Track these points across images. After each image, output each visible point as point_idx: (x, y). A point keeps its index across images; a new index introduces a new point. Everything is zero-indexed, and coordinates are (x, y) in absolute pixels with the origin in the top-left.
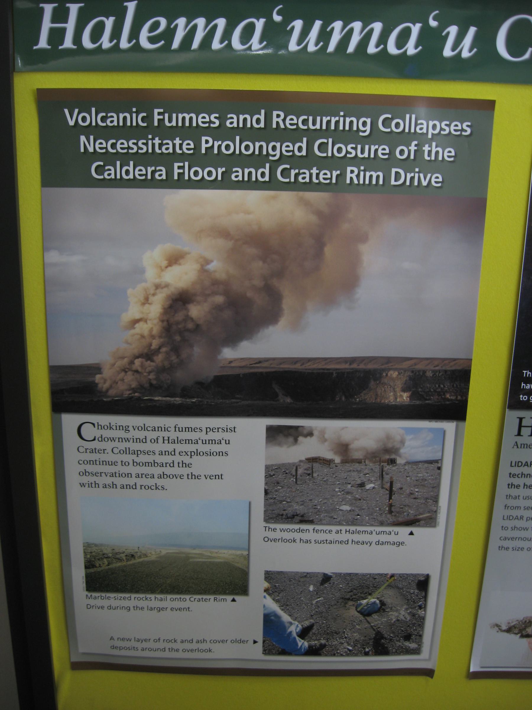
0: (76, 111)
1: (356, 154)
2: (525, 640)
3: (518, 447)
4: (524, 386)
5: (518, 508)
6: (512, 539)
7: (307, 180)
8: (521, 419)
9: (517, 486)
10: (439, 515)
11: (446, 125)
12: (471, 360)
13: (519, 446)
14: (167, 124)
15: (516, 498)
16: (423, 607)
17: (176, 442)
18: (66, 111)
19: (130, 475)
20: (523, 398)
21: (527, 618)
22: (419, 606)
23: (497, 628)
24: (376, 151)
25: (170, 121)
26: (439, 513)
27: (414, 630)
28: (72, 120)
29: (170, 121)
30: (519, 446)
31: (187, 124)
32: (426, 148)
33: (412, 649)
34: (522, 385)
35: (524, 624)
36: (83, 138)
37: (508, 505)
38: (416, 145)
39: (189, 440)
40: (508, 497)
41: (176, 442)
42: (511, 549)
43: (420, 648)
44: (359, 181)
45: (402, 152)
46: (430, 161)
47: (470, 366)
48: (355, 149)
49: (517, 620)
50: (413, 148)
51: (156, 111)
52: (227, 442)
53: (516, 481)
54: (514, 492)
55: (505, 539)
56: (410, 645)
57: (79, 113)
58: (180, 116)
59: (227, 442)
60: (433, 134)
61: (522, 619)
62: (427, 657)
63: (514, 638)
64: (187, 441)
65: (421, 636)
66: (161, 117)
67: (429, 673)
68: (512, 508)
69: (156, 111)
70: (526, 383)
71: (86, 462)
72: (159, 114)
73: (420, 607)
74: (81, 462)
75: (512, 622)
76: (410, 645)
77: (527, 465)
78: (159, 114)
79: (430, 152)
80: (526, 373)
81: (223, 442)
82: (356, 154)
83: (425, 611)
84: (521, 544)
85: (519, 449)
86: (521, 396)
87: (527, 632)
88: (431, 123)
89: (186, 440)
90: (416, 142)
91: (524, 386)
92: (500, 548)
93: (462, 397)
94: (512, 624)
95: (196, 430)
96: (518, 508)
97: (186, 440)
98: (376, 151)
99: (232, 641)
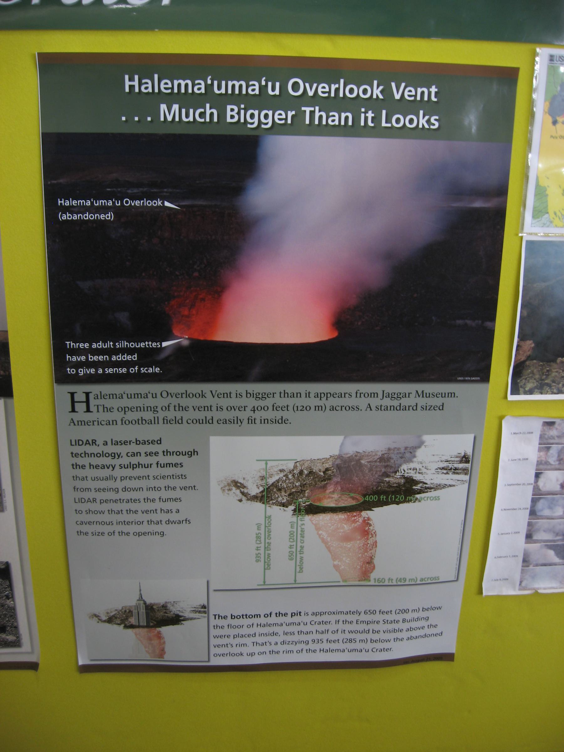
0: (403, 85)
2: (130, 631)
3: (75, 425)
4: (69, 358)
5: (89, 489)
6: (89, 523)
8: (72, 394)
9: (82, 467)
10: (4, 499)
12: (7, 331)
13: (76, 423)
14: (216, 91)
15: (83, 479)
16: (11, 596)
17: (99, 397)
18: (393, 84)
20: (71, 371)
21: (125, 607)
22: (5, 595)
23: (97, 619)
25: (219, 88)
26: (5, 497)
27: (7, 621)
28: (398, 93)
29: (219, 88)
30: (76, 423)
31: (183, 91)
33: (11, 642)
34: (68, 357)
35: (124, 614)
36: (163, 107)
37: (76, 487)
39: (138, 394)
40: (75, 478)
41: (99, 397)
42: (90, 534)
43: (19, 640)
47: (7, 339)
49: (116, 610)
50: (136, 368)
52: (154, 396)
53: (80, 461)
54: (80, 473)
55: (82, 523)
56: (8, 637)
58: (230, 84)
59: (154, 396)
61: (120, 608)
62: (29, 650)
63: (117, 630)
64: (111, 396)
65: (16, 628)
67: (33, 666)
68: (82, 490)
70: (71, 355)
73: (8, 597)
75: (111, 612)
76: (8, 637)
77: (89, 444)
80: (70, 344)
81: (150, 396)
83: (14, 600)
84: (100, 528)
85: (77, 427)
86: (68, 369)
87: (130, 622)
91: (69, 358)
92: (79, 533)
93: (4, 372)
94: (112, 614)
96: (89, 489)
99: (141, 594)
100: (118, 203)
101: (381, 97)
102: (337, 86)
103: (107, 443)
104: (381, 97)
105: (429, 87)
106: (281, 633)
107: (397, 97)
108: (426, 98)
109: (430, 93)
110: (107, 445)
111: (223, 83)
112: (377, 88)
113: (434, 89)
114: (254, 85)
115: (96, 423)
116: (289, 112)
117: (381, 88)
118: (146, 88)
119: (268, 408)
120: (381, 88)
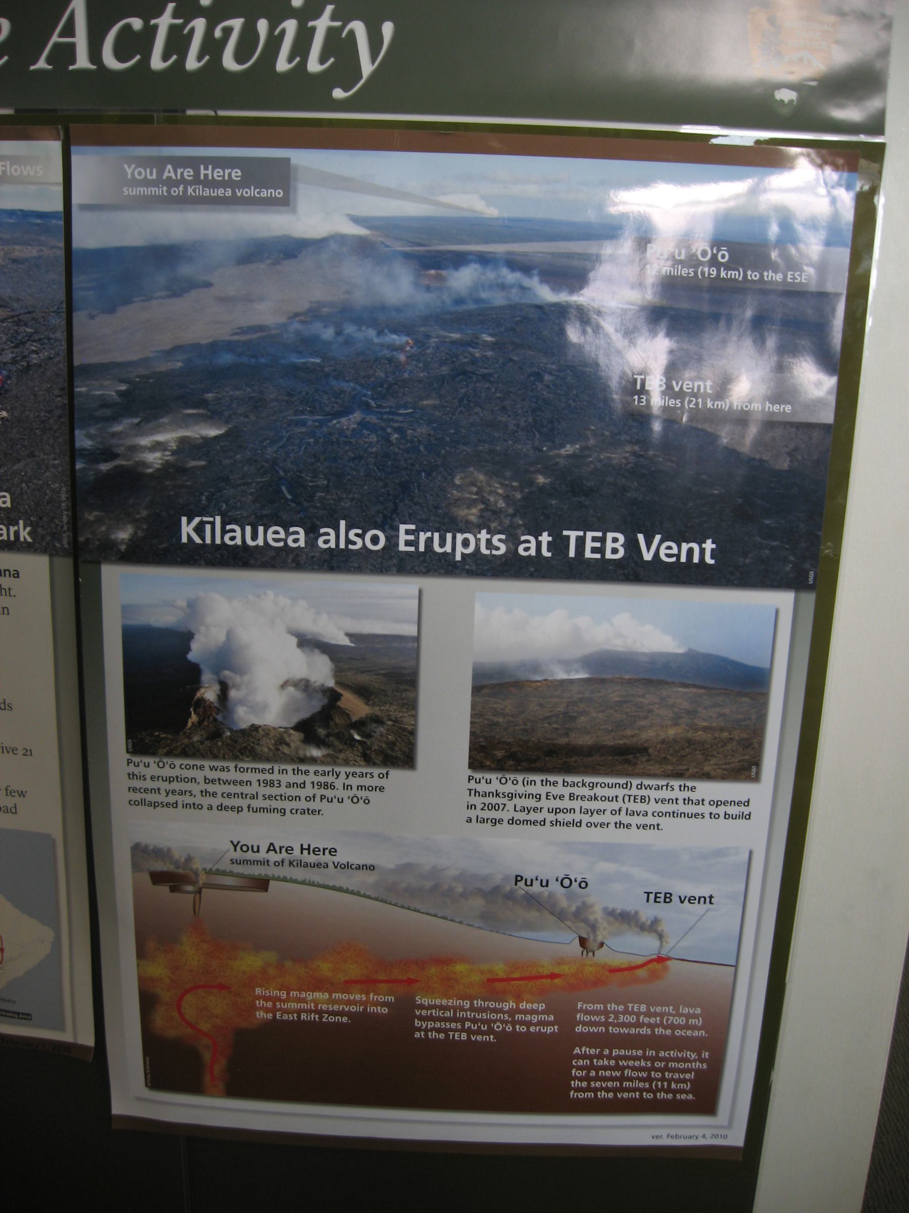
0: (658, 538)
1: (364, 543)
7: (533, 552)
11: (357, 535)
18: (641, 537)
28: (648, 549)
44: (203, 539)
48: (349, 542)
51: (403, 528)
57: (662, 541)
66: (412, 537)
69: (403, 528)
72: (408, 532)
78: (408, 532)
82: (364, 543)
101: (29, 540)
102: (16, 528)
104: (29, 540)
105: (701, 542)
106: (201, 779)
107: (648, 556)
108: (696, 560)
109: (702, 551)
111: (449, 536)
113: (709, 545)
114: (528, 541)
117: (28, 529)
120: (28, 529)
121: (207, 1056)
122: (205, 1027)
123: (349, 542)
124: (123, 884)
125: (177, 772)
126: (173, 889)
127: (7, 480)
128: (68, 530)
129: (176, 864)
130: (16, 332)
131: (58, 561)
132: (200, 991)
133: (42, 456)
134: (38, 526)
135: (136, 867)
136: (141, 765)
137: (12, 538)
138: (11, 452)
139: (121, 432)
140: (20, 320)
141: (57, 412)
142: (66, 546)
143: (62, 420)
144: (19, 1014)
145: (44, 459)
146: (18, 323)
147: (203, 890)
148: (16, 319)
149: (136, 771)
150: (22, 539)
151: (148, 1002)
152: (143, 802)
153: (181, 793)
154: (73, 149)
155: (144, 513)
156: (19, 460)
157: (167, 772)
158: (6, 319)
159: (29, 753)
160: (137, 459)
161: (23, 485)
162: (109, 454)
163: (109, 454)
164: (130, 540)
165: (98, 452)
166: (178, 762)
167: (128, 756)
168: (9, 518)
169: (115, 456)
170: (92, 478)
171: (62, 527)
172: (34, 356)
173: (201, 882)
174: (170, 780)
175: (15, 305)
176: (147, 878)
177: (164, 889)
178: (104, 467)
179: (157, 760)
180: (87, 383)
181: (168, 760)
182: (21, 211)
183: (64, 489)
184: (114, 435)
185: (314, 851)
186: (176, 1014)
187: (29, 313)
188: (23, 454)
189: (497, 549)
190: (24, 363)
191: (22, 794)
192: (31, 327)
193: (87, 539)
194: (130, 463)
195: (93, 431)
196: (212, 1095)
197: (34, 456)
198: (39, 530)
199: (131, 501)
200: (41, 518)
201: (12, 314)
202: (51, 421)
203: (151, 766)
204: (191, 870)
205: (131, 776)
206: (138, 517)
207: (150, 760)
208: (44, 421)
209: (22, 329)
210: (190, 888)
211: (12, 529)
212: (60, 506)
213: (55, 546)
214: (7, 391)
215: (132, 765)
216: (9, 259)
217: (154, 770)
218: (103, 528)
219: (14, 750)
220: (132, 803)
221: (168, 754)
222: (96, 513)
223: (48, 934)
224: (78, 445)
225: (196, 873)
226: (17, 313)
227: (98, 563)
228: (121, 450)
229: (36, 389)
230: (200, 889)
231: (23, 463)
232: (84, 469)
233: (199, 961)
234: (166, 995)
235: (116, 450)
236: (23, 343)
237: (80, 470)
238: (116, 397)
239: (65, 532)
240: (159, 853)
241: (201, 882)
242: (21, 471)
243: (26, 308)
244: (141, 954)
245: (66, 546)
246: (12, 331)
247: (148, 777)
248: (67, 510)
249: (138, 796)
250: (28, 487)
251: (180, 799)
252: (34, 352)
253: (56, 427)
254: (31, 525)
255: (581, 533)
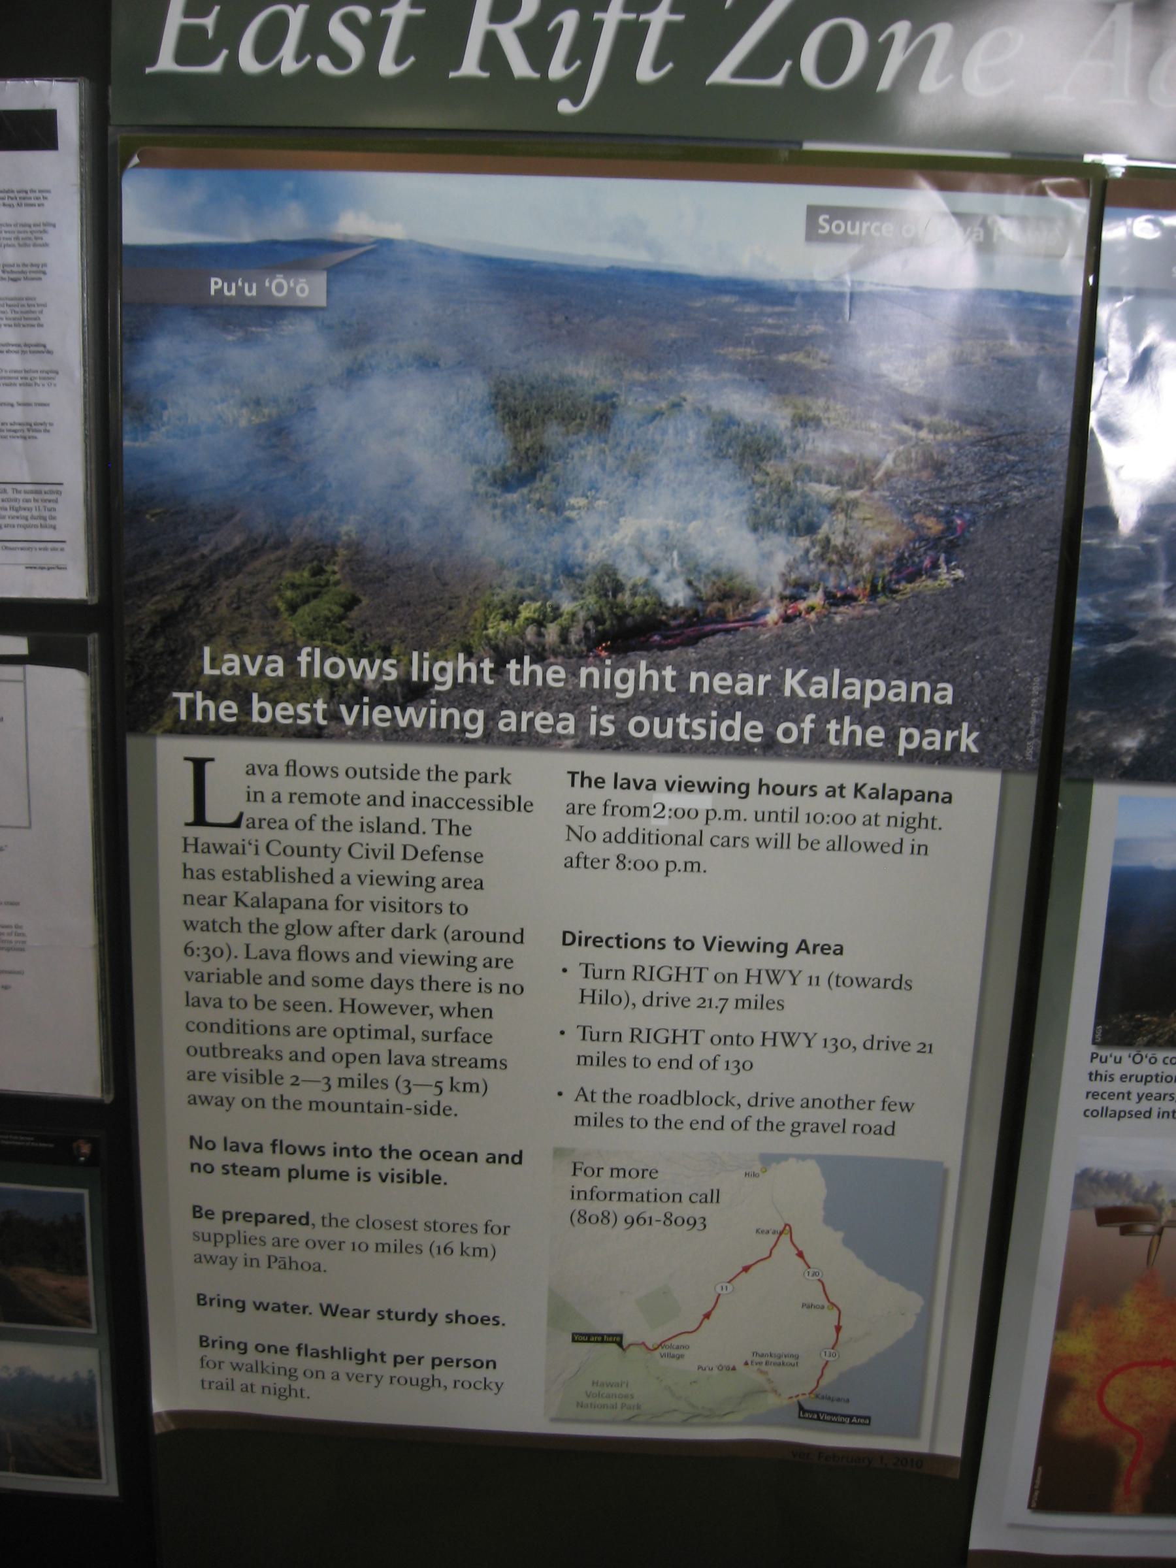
19: (260, 1103)
24: (531, 722)
32: (833, 726)
38: (812, 721)
45: (787, 733)
46: (839, 747)
50: (807, 725)
60: (873, 703)
64: (315, 798)
71: (202, 1027)
74: (192, 1027)
79: (839, 734)
88: (869, 684)
89: (312, 795)
90: (813, 716)
95: (375, 1085)
97: (312, 795)
98: (531, 722)
100: (250, 290)
101: (974, 749)
102: (956, 733)
103: (261, 1147)
104: (974, 749)
110: (261, 1151)
112: (968, 735)
115: (214, 978)
116: (948, 733)
117: (975, 735)
118: (931, 743)
119: (188, 1051)
120: (975, 735)
121: (1126, 1459)
122: (1132, 1420)
123: (599, 728)
124: (1053, 1225)
125: (1159, 1068)
126: (1125, 1231)
127: (952, 666)
128: (1036, 736)
129: (1135, 1196)
130: (993, 460)
131: (1016, 779)
132: (1136, 1371)
133: (1010, 633)
134: (990, 730)
135: (1078, 1201)
136: (1111, 1060)
137: (948, 747)
138: (963, 627)
139: (1143, 601)
140: (999, 444)
141: (1041, 573)
142: (1031, 759)
143: (1047, 583)
144: (851, 1417)
145: (1012, 638)
146: (997, 448)
147: (1167, 1231)
148: (994, 442)
149: (1102, 1068)
150: (963, 749)
151: (1058, 1388)
152: (1104, 1112)
153: (1160, 1097)
154: (1108, 211)
155: (1163, 713)
156: (975, 639)
157: (1145, 1069)
158: (979, 441)
159: (927, 1049)
160: (1162, 639)
161: (976, 673)
162: (1121, 631)
163: (1121, 631)
164: (1140, 750)
165: (1107, 628)
166: (1161, 1054)
167: (1094, 1049)
168: (947, 719)
169: (1133, 634)
170: (1093, 664)
171: (1028, 732)
172: (1015, 494)
173: (1164, 1220)
174: (1146, 1080)
175: (995, 423)
176: (1091, 1217)
177: (1113, 1231)
178: (1113, 649)
179: (1133, 1053)
180: (1101, 533)
181: (1148, 1053)
182: (1020, 293)
183: (1037, 680)
184: (1133, 605)
185: (433, 1179)
186: (1095, 1405)
187: (1014, 434)
188: (980, 629)
189: (697, 733)
190: (1000, 504)
191: (907, 1107)
192: (1017, 454)
193: (1077, 749)
194: (1151, 643)
195: (1102, 599)
196: (1123, 1514)
197: (998, 633)
198: (992, 736)
199: (1147, 697)
200: (996, 720)
201: (989, 434)
202: (1030, 585)
203: (1123, 1062)
204: (1154, 1203)
205: (1094, 1076)
206: (1154, 717)
207: (1124, 1053)
208: (1019, 585)
209: (1002, 456)
210: (1148, 1228)
211: (950, 735)
212: (1028, 703)
213: (1011, 758)
214: (967, 542)
215: (1097, 1061)
216: (993, 358)
217: (1128, 1067)
218: (1102, 734)
219: (904, 1046)
220: (1088, 1113)
221: (1151, 1044)
222: (1093, 713)
223: (915, 1301)
224: (1079, 617)
225: (1160, 1208)
226: (997, 433)
227: (1090, 782)
228: (1139, 626)
229: (1013, 539)
230: (1162, 1229)
231: (980, 642)
232: (1083, 651)
233: (1141, 1329)
234: (1085, 1379)
235: (1132, 626)
236: (1000, 475)
237: (1079, 653)
238: (1141, 553)
239: (1031, 739)
240: (1114, 1182)
241: (1164, 1220)
242: (975, 653)
243: (1012, 427)
244: (1063, 1322)
245: (1031, 759)
246: (985, 459)
247: (1117, 1078)
248: (1038, 709)
249: (1098, 1104)
250: (983, 676)
251: (1156, 1105)
252: (1015, 488)
253: (1036, 593)
254: (980, 728)
255: (191, 695)
